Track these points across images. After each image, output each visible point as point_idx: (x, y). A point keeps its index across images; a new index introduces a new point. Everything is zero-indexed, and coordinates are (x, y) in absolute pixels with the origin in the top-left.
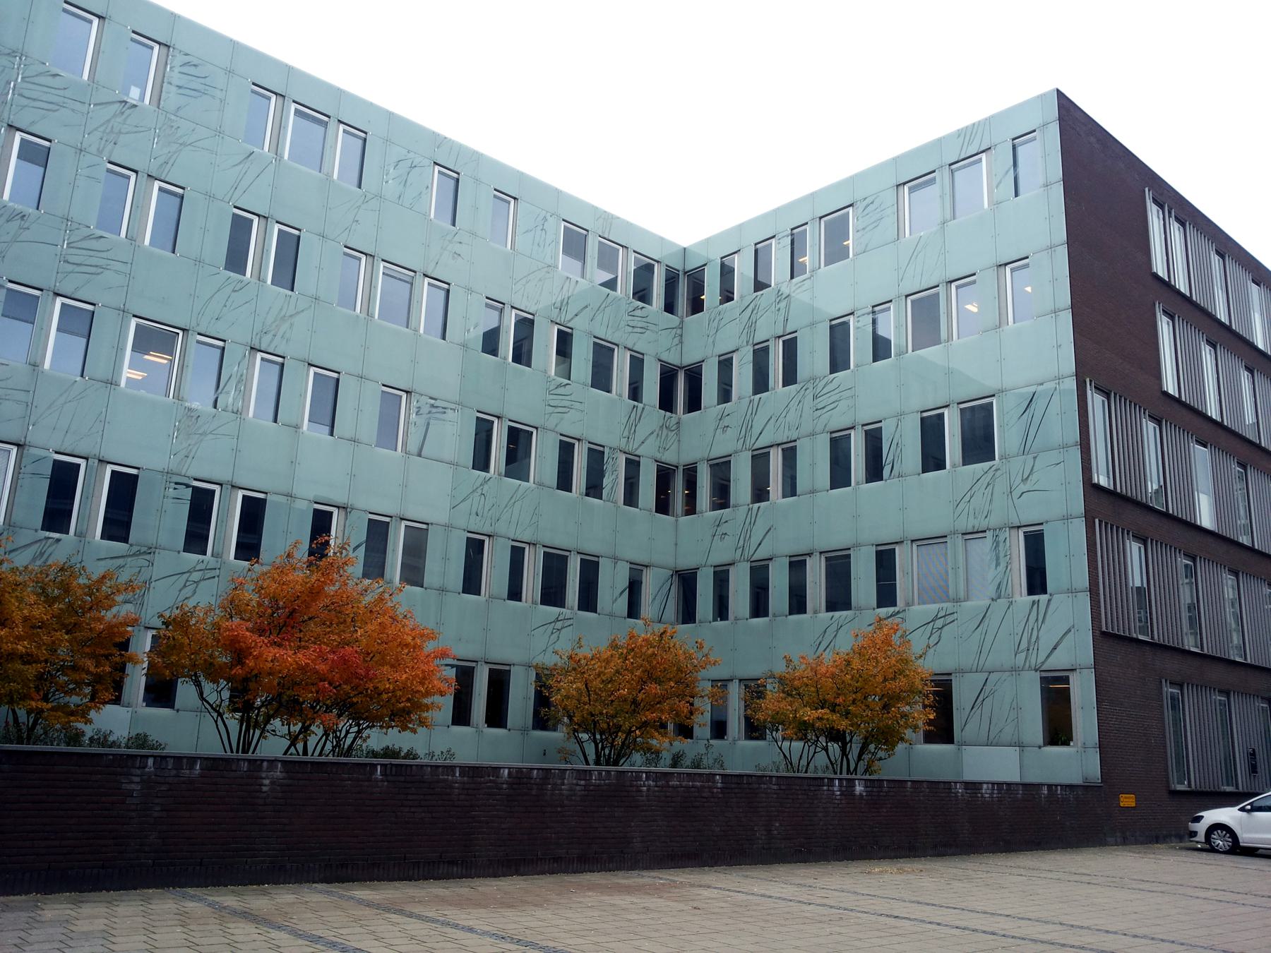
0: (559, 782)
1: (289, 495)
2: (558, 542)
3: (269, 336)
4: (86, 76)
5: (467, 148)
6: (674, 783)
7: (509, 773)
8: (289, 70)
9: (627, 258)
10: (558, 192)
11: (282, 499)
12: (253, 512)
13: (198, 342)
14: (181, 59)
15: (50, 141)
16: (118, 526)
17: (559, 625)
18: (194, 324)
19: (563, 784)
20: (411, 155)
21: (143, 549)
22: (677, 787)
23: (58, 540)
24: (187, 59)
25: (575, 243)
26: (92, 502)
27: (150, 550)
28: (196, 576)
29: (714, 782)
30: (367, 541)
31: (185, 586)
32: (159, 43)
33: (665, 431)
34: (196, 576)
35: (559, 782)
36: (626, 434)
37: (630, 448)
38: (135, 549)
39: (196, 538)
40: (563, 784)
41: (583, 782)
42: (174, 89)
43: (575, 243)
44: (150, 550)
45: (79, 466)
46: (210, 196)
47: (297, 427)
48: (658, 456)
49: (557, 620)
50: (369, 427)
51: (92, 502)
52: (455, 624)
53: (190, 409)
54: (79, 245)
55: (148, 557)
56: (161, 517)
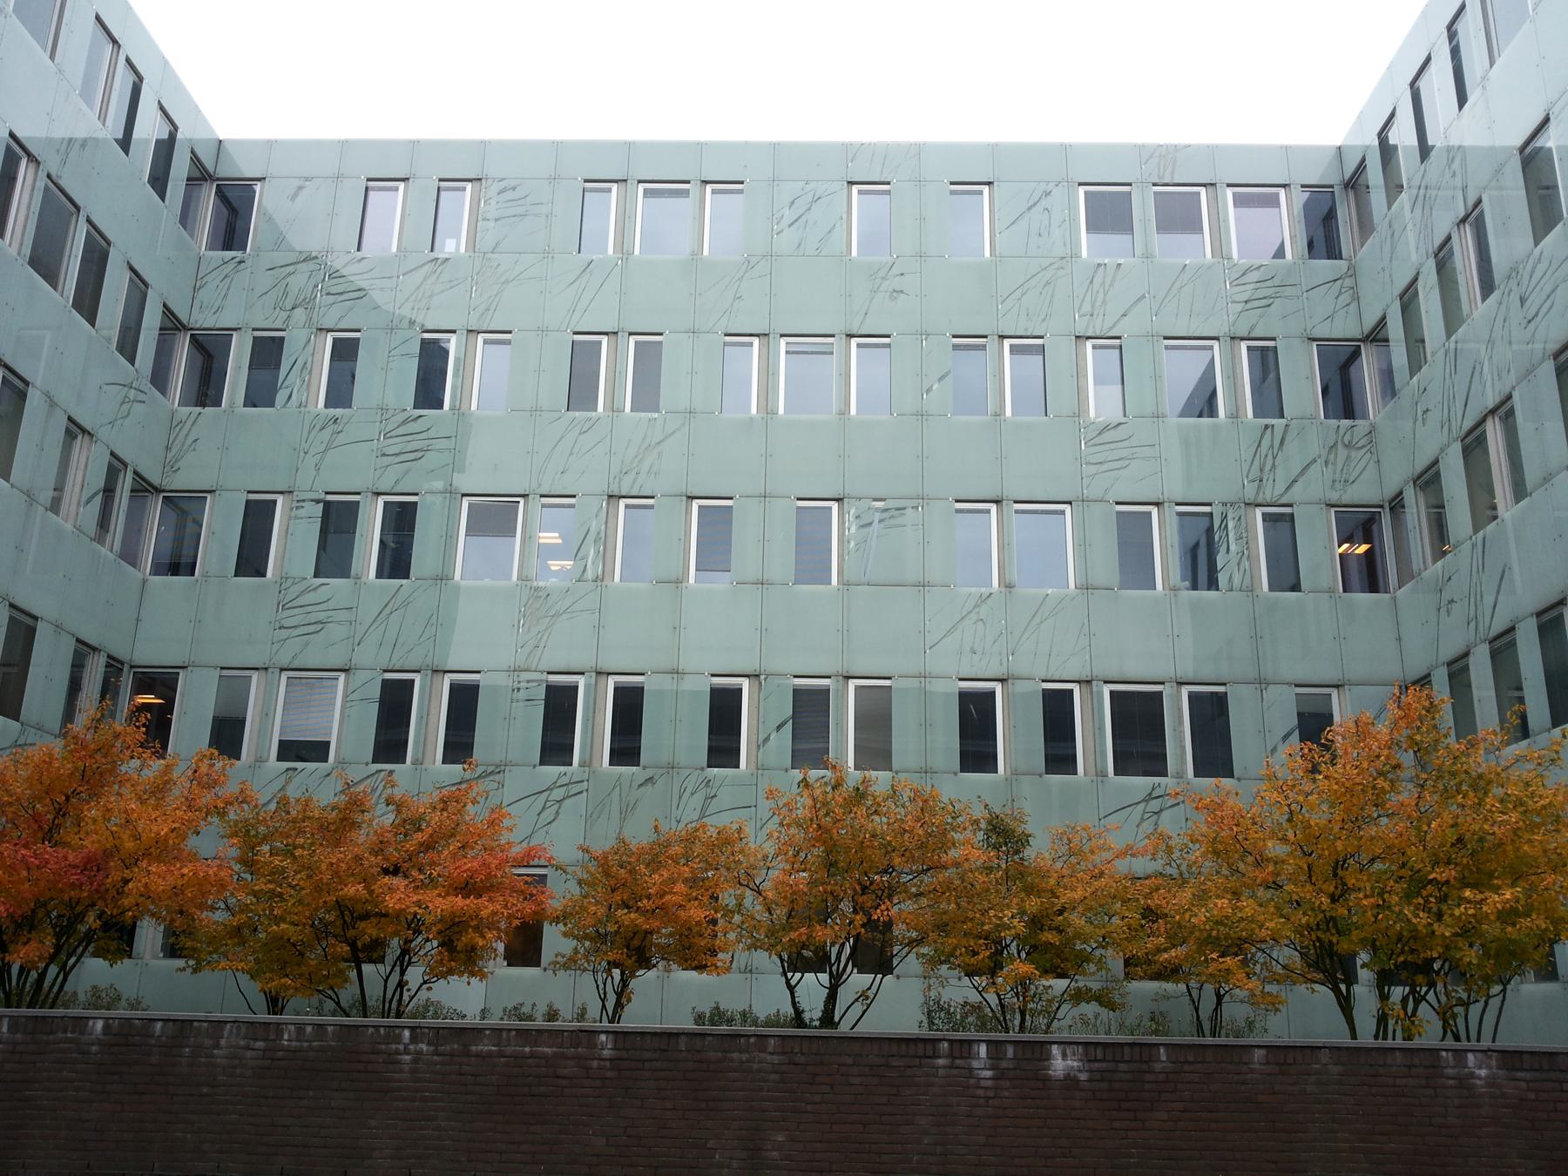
0: (208, 1042)
1: (676, 672)
2: (1134, 669)
3: (632, 476)
4: (987, 254)
5: (898, 145)
6: (485, 1047)
7: (106, 1027)
8: (629, 147)
9: (1215, 202)
10: (1065, 148)
11: (913, 683)
12: (629, 706)
13: (1017, 512)
14: (496, 187)
15: (1274, 339)
16: (459, 745)
17: (1154, 805)
18: (534, 485)
19: (217, 1046)
20: (813, 185)
21: (490, 769)
22: (490, 1055)
23: (391, 772)
24: (503, 184)
25: (1109, 212)
26: (429, 721)
27: (499, 769)
28: (558, 794)
29: (593, 1046)
30: (793, 717)
31: (544, 808)
32: (1204, 185)
33: (1342, 452)
34: (558, 794)
35: (208, 1042)
36: (1255, 473)
37: (1268, 494)
38: (480, 770)
39: (556, 745)
40: (217, 1046)
41: (260, 1044)
42: (492, 224)
43: (1109, 212)
44: (499, 769)
45: (992, 694)
46: (542, 331)
47: (679, 581)
48: (1334, 497)
49: (1150, 797)
50: (782, 561)
51: (429, 721)
52: (1102, 822)
53: (537, 589)
54: (1098, 440)
55: (497, 778)
56: (510, 729)
